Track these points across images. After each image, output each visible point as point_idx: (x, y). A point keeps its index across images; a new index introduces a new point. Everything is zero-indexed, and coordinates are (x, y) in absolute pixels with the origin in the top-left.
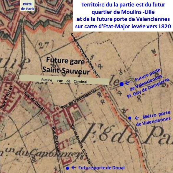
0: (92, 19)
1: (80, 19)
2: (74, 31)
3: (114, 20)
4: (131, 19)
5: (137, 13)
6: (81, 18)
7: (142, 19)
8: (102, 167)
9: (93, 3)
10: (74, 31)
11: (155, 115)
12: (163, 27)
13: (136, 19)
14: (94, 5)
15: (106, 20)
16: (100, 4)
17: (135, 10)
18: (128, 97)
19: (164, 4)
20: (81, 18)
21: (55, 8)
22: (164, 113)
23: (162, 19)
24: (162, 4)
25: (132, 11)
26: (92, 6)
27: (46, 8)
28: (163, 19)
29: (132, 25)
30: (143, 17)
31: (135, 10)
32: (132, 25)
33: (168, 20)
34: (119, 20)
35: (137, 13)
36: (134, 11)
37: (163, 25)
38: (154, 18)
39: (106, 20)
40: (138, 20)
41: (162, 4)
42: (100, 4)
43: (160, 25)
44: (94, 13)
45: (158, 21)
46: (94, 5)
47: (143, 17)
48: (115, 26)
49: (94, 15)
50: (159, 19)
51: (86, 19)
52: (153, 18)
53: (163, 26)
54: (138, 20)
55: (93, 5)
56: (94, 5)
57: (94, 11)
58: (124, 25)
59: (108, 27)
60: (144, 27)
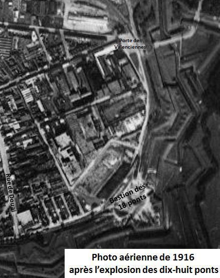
3: (196, 272)
4: (75, 270)
9: (189, 267)
14: (111, 258)
17: (166, 267)
18: (93, 258)
21: (26, 65)
22: (81, 269)
23: (148, 256)
25: (185, 269)
26: (210, 272)
27: (137, 168)
28: (150, 257)
30: (117, 267)
31: (166, 267)
33: (89, 271)
34: (204, 272)
38: (129, 269)
43: (175, 255)
45: (143, 260)
46: (111, 258)
47: (117, 267)
48: (175, 269)
49: (99, 254)
52: (127, 268)
55: (189, 270)
56: (111, 258)
60: (122, 258)
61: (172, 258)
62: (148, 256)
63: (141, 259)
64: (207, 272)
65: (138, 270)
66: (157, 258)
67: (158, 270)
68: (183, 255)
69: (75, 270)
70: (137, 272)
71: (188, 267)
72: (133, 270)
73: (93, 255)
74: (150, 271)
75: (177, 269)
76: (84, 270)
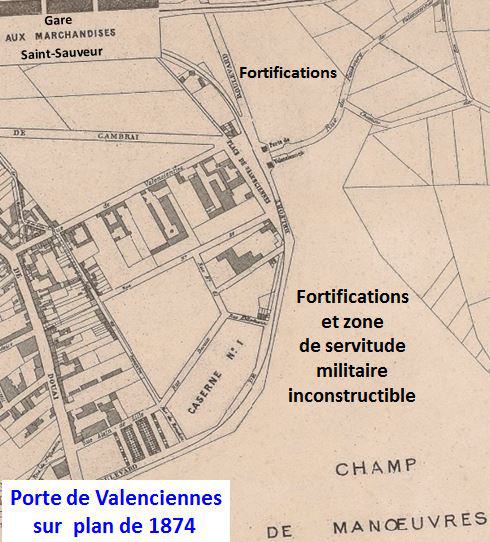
0: (91, 526)
1: (332, 321)
2: (227, 483)
4: (75, 500)
5: (105, 528)
6: (335, 319)
7: (116, 499)
8: (46, 495)
9: (366, 341)
10: (227, 483)
11: (272, 532)
12: (166, 529)
13: (93, 498)
15: (379, 348)
16: (373, 369)
17: (346, 364)
19: (57, 524)
20: (335, 319)
22: (37, 496)
23: (192, 496)
24: (51, 523)
29: (97, 492)
31: (346, 364)
32: (97, 492)
34: (360, 325)
35: (105, 528)
36: (343, 366)
37: (166, 522)
38: (368, 369)
39: (379, 348)
40: (102, 503)
41: (51, 523)
42: (373, 369)
43: (154, 520)
44: (392, 394)
50: (183, 498)
51: (307, 344)
52: (159, 494)
53: (167, 525)
54: (102, 503)
55: (348, 370)
57: (392, 400)
58: (368, 364)
59: (354, 372)
61: (148, 526)
62: (192, 496)
63: (344, 348)
64: (393, 301)
65: (108, 526)
66: (88, 498)
67: (323, 347)
68: (51, 504)
69: (75, 500)
70: (365, 327)
71: (364, 339)
72: (385, 298)
73: (13, 492)
74: (98, 528)
75: (150, 206)
76: (379, 372)
